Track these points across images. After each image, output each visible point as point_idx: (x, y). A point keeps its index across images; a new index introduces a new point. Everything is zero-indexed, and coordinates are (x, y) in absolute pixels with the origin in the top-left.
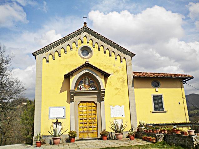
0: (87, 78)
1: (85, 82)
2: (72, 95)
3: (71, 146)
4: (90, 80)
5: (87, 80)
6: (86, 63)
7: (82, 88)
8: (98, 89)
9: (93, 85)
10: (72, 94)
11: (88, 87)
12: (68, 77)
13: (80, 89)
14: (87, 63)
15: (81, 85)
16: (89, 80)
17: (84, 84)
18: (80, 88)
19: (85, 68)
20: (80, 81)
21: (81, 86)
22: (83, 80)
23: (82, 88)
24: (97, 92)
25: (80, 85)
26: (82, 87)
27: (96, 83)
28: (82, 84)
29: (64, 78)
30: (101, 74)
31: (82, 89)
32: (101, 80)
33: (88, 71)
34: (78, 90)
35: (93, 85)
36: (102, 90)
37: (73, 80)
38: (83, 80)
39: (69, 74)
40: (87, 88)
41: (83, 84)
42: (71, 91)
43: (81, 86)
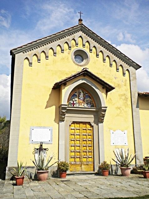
0: (81, 91)
1: (79, 96)
2: (64, 112)
4: (86, 94)
5: (82, 93)
6: (85, 69)
7: (75, 104)
9: (89, 101)
10: (63, 111)
11: (83, 102)
12: (58, 87)
13: (72, 105)
14: (86, 71)
15: (73, 100)
16: (84, 95)
17: (77, 99)
21: (73, 101)
22: (76, 94)
24: (95, 110)
26: (75, 102)
28: (75, 99)
31: (75, 105)
33: (85, 82)
35: (89, 101)
36: (103, 109)
37: (66, 91)
38: (76, 94)
40: (81, 105)
41: (77, 99)
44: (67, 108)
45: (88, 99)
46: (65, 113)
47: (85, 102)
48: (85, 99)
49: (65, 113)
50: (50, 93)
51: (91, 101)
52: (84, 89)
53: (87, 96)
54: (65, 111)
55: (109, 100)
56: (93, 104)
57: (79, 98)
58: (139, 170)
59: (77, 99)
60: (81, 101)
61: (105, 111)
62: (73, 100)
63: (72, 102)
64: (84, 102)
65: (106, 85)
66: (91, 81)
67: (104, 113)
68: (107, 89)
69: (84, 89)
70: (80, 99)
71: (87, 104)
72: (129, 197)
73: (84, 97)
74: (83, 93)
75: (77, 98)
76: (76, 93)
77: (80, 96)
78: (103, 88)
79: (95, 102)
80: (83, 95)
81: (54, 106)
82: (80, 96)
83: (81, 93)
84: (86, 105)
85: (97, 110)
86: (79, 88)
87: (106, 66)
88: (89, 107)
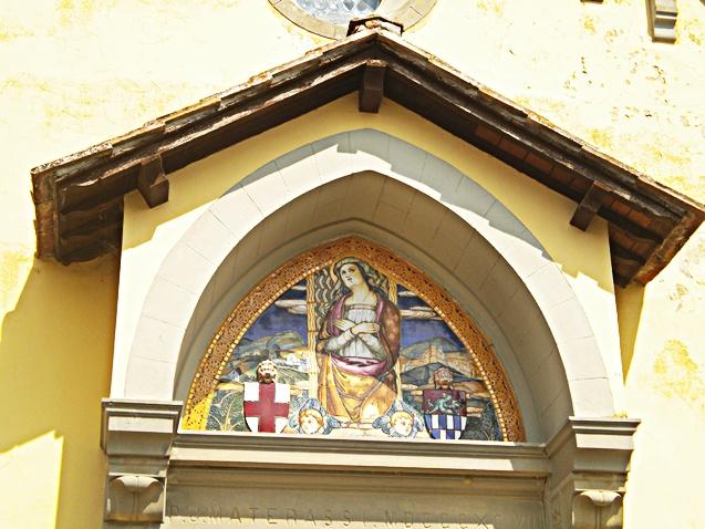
0: (353, 280)
1: (329, 330)
2: (138, 493)
3: (474, 484)
4: (406, 302)
5: (363, 297)
6: (363, 33)
7: (284, 410)
8: (519, 434)
9: (444, 376)
10: (129, 479)
11: (370, 394)
12: (88, 214)
13: (253, 422)
14: (376, 45)
15: (267, 367)
16: (384, 309)
17: (310, 355)
18: (250, 409)
19: (353, 123)
20: (265, 292)
21: (265, 381)
22: (299, 306)
23: (284, 410)
24: (505, 465)
25: (256, 361)
26: (282, 394)
27: (486, 349)
28: (291, 359)
29: (39, 255)
30: (563, 210)
31: (280, 423)
32: (565, 284)
33: (384, 168)
34: (226, 430)
35: (444, 376)
36: (583, 441)
37: (174, 257)
38: (299, 306)
39: (103, 159)
40: (355, 417)
41: (306, 359)
42: (116, 424)
43: (265, 381)
44: (177, 454)
45: (435, 354)
46: (152, 507)
47: (400, 386)
48: (394, 357)
49: (152, 507)
50: (12, 307)
51: (456, 375)
52: (386, 255)
53: (424, 321)
54: (146, 480)
55: (659, 367)
56: (487, 403)
57: (334, 344)
58: (375, 68)
59: (306, 359)
60: (355, 380)
61: (614, 467)
62: (267, 367)
63: (252, 392)
64: (391, 384)
65: (609, 187)
66: (426, 148)
67: (610, 496)
68: (620, 236)
69: (386, 255)
70: (335, 354)
71: (425, 408)
72: (81, 263)
73: (381, 335)
74: (372, 299)
75: (306, 345)
76: (302, 295)
77: (344, 325)
78: (580, 223)
79: (504, 387)
80: (381, 322)
81: (51, 434)
82: (344, 325)
83: (348, 293)
84: (404, 425)
85: (527, 466)
86: (321, 252)
87: (613, 34)
88: (443, 439)
